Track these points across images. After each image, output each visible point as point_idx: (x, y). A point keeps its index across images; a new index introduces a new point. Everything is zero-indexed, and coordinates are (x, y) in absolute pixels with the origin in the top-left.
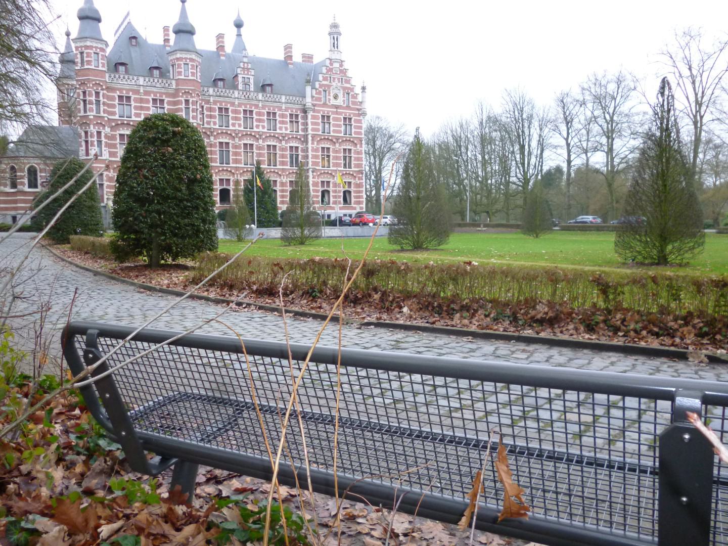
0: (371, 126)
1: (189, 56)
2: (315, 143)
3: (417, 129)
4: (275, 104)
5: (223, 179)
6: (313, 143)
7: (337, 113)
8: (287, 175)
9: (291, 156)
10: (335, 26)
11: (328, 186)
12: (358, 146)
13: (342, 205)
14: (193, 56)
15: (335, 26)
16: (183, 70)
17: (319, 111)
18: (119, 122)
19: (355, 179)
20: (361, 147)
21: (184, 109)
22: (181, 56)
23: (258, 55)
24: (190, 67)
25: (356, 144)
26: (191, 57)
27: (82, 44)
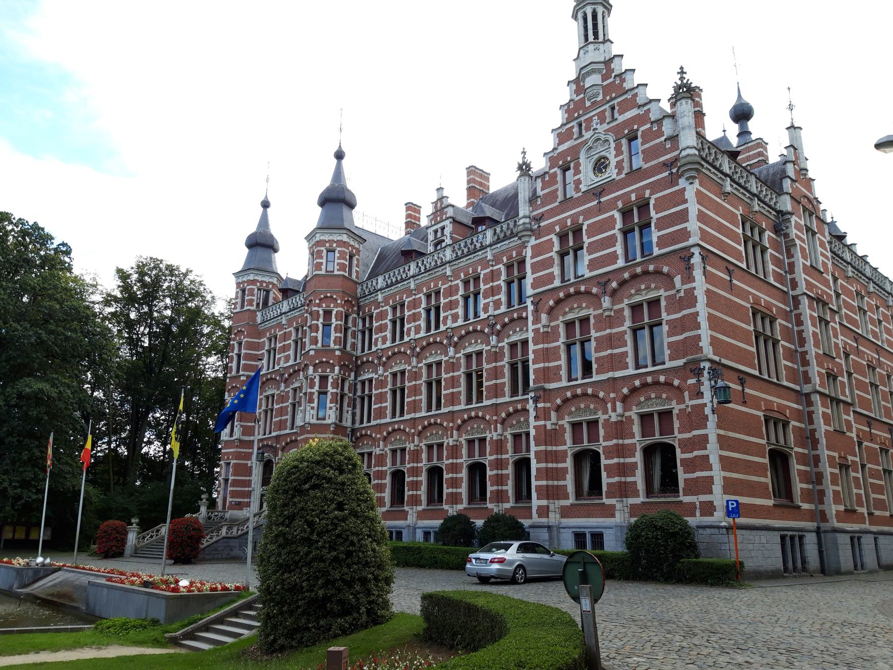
0: (845, 236)
1: (336, 238)
2: (544, 317)
3: (682, 72)
4: (474, 258)
5: (650, 415)
6: (537, 320)
7: (601, 209)
8: (503, 422)
9: (513, 367)
10: (878, 146)
11: (666, 429)
12: (678, 280)
13: (571, 500)
14: (345, 238)
15: (878, 146)
16: (324, 261)
17: (550, 229)
18: (637, 383)
19: (681, 401)
20: (689, 278)
21: (321, 326)
22: (323, 238)
23: (873, 261)
24: (337, 255)
25: (669, 277)
26: (339, 238)
27: (245, 279)
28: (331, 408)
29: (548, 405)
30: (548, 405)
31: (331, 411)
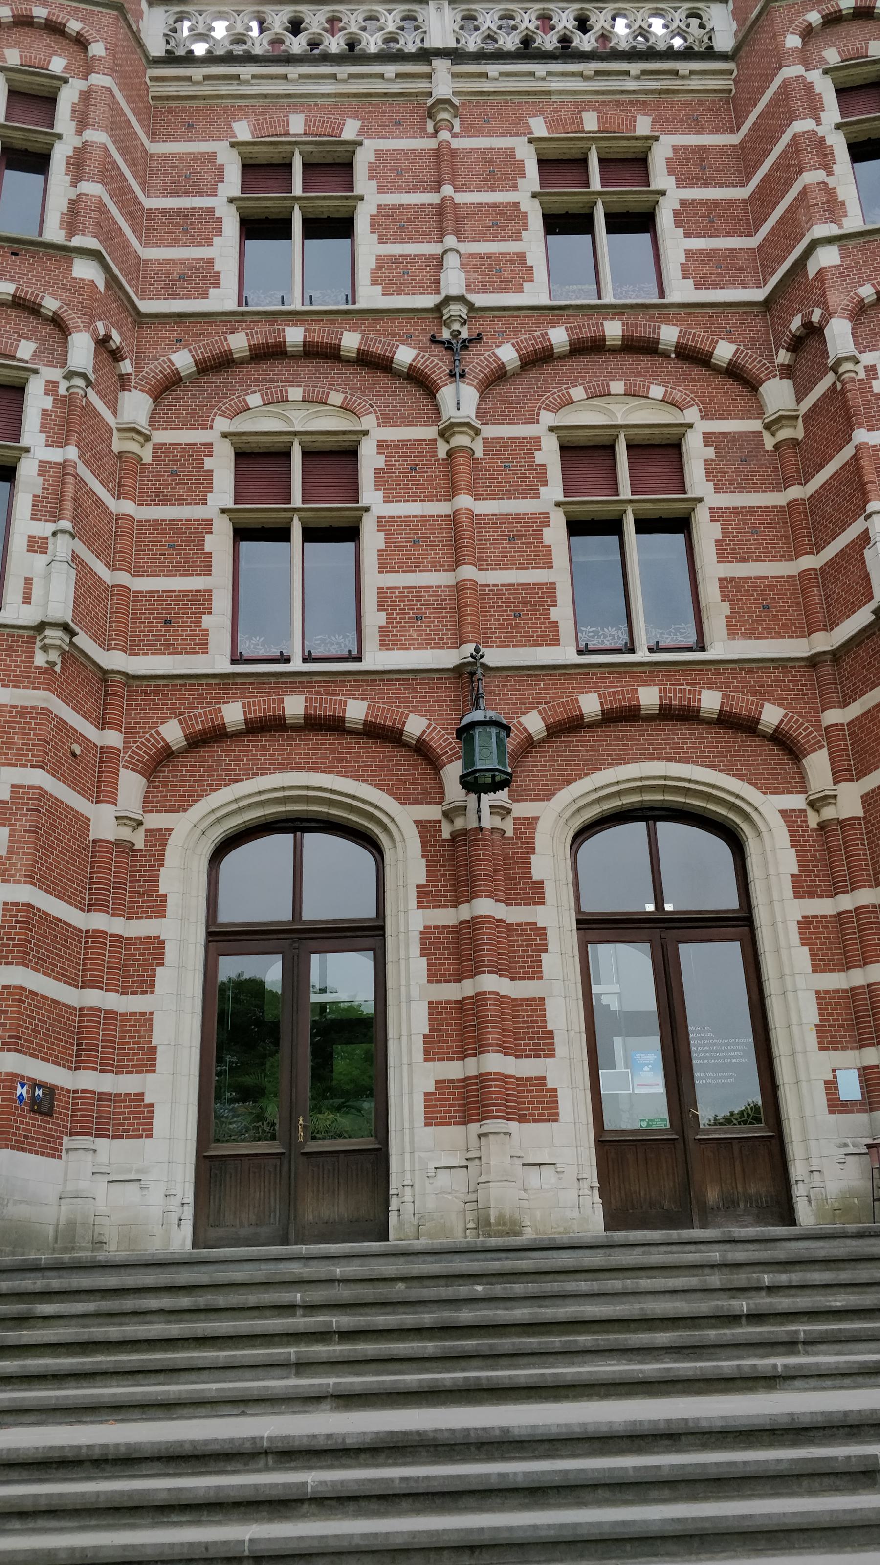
28: (37, 545)
29: (113, 738)
30: (113, 738)
31: (40, 560)
